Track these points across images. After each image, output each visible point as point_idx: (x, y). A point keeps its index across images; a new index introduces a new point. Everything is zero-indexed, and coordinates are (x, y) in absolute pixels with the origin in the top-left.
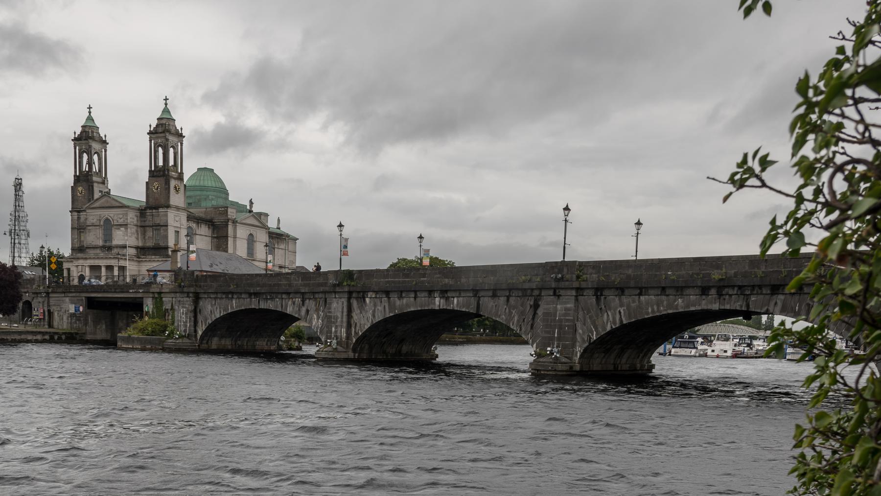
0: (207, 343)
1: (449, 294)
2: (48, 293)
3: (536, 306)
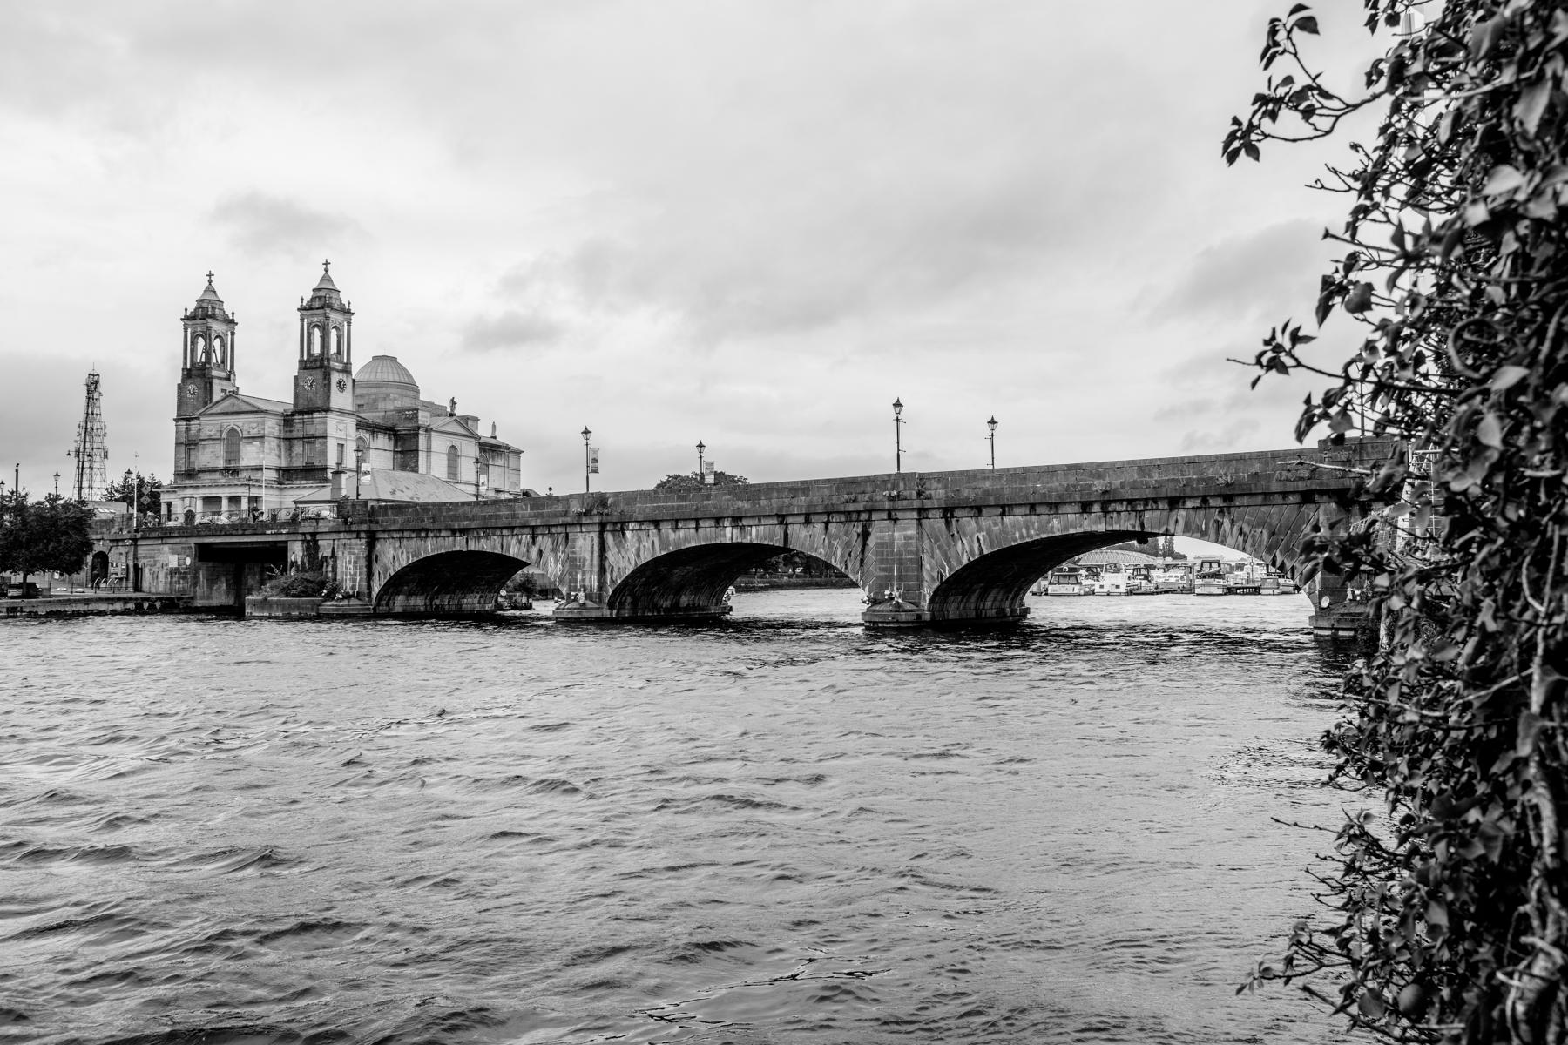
1: (745, 522)
2: (135, 540)
3: (865, 535)
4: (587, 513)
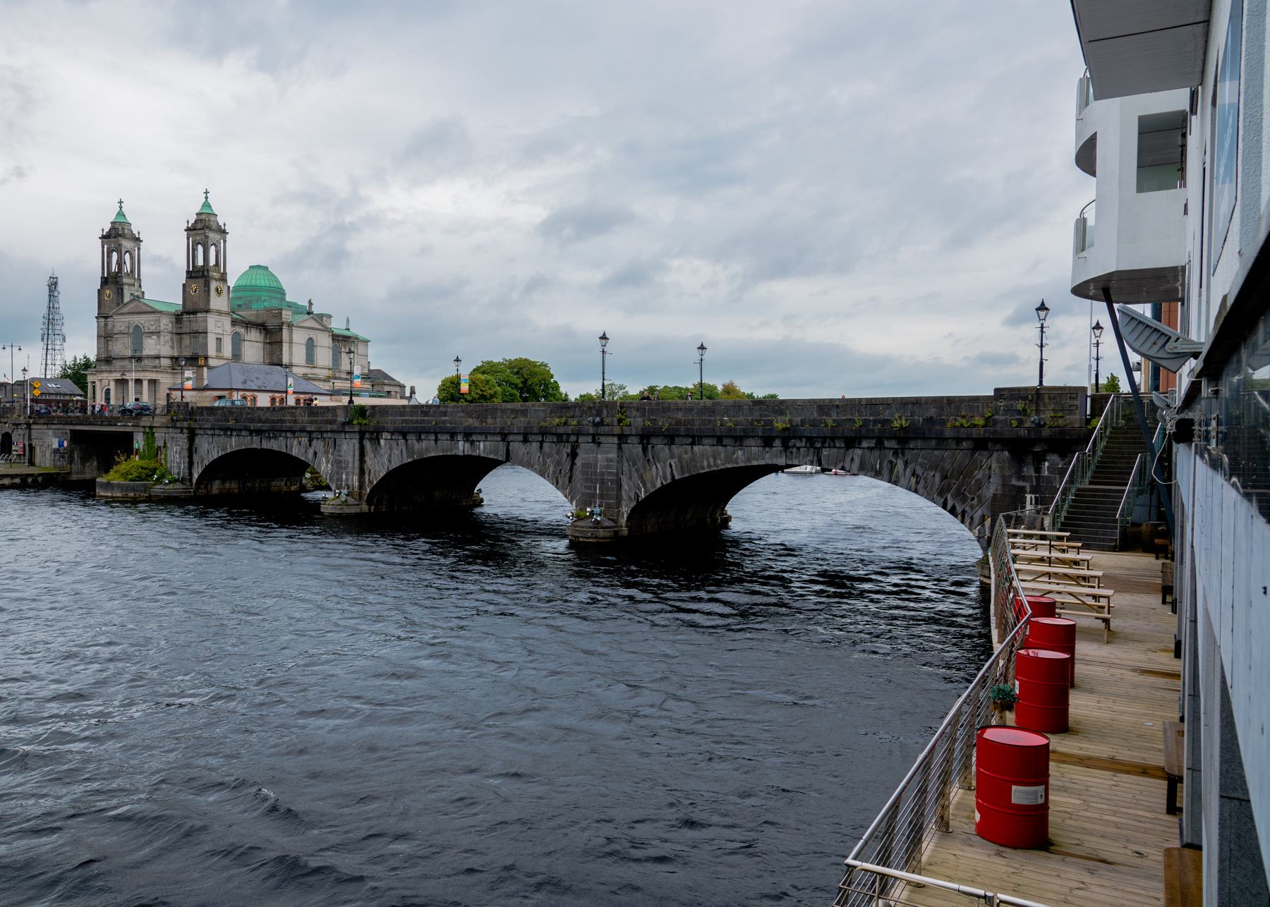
0: (206, 488)
1: (474, 438)
2: (29, 425)
3: (573, 455)
4: (350, 423)
